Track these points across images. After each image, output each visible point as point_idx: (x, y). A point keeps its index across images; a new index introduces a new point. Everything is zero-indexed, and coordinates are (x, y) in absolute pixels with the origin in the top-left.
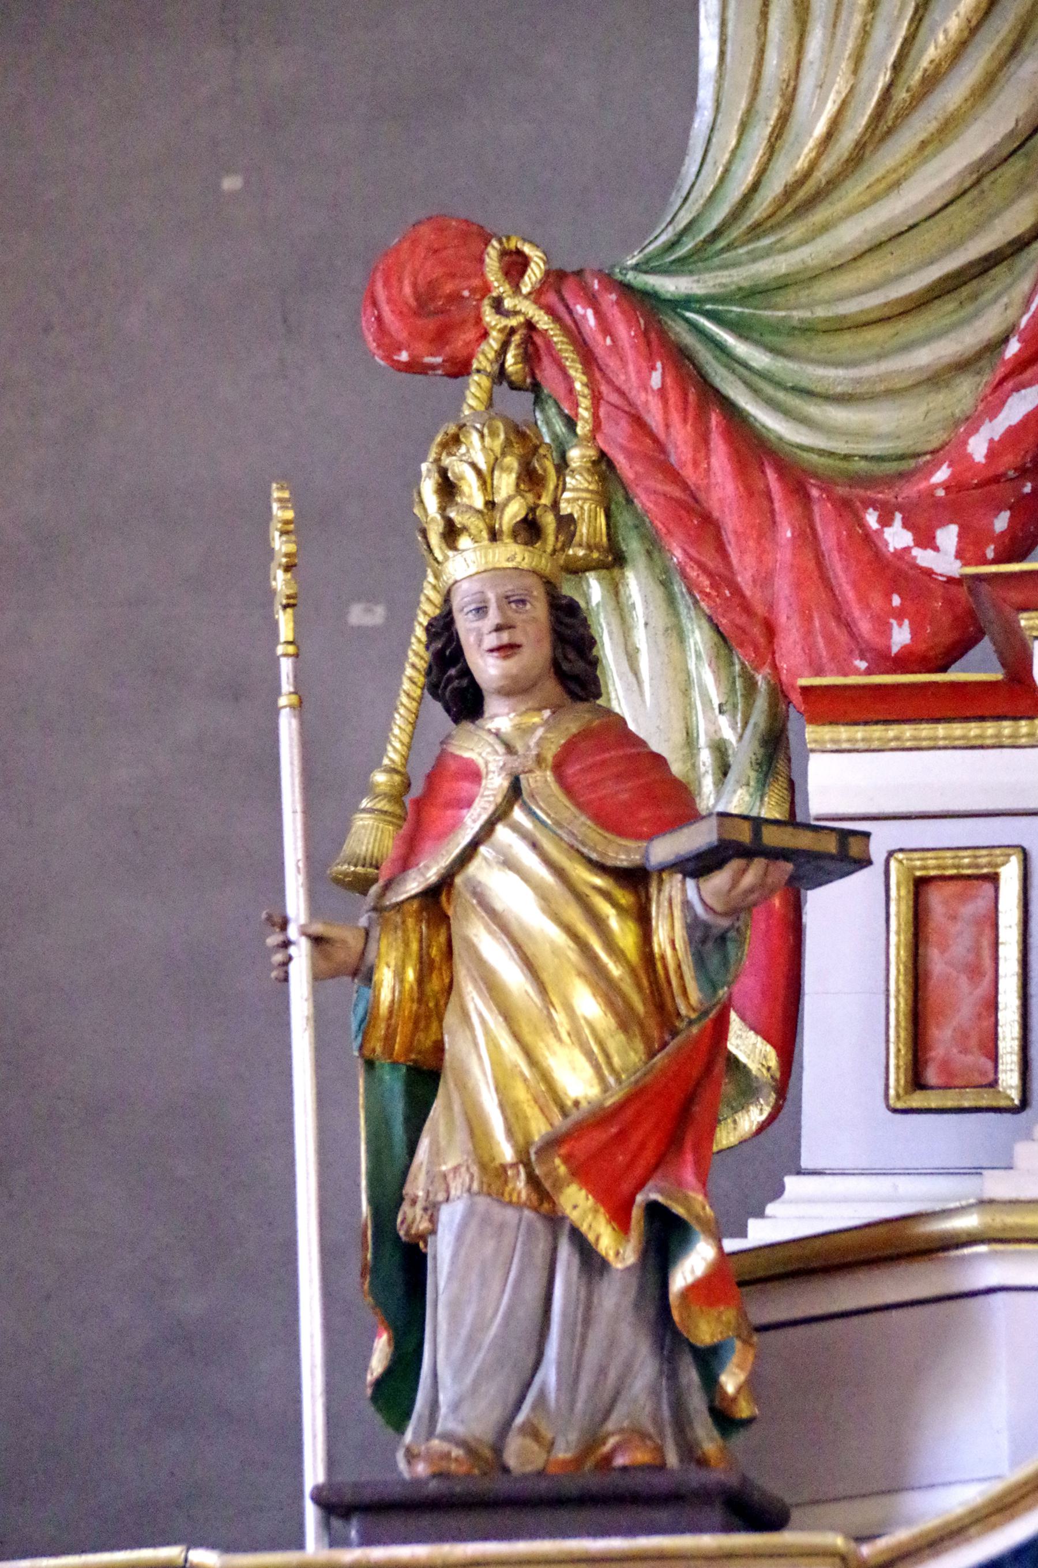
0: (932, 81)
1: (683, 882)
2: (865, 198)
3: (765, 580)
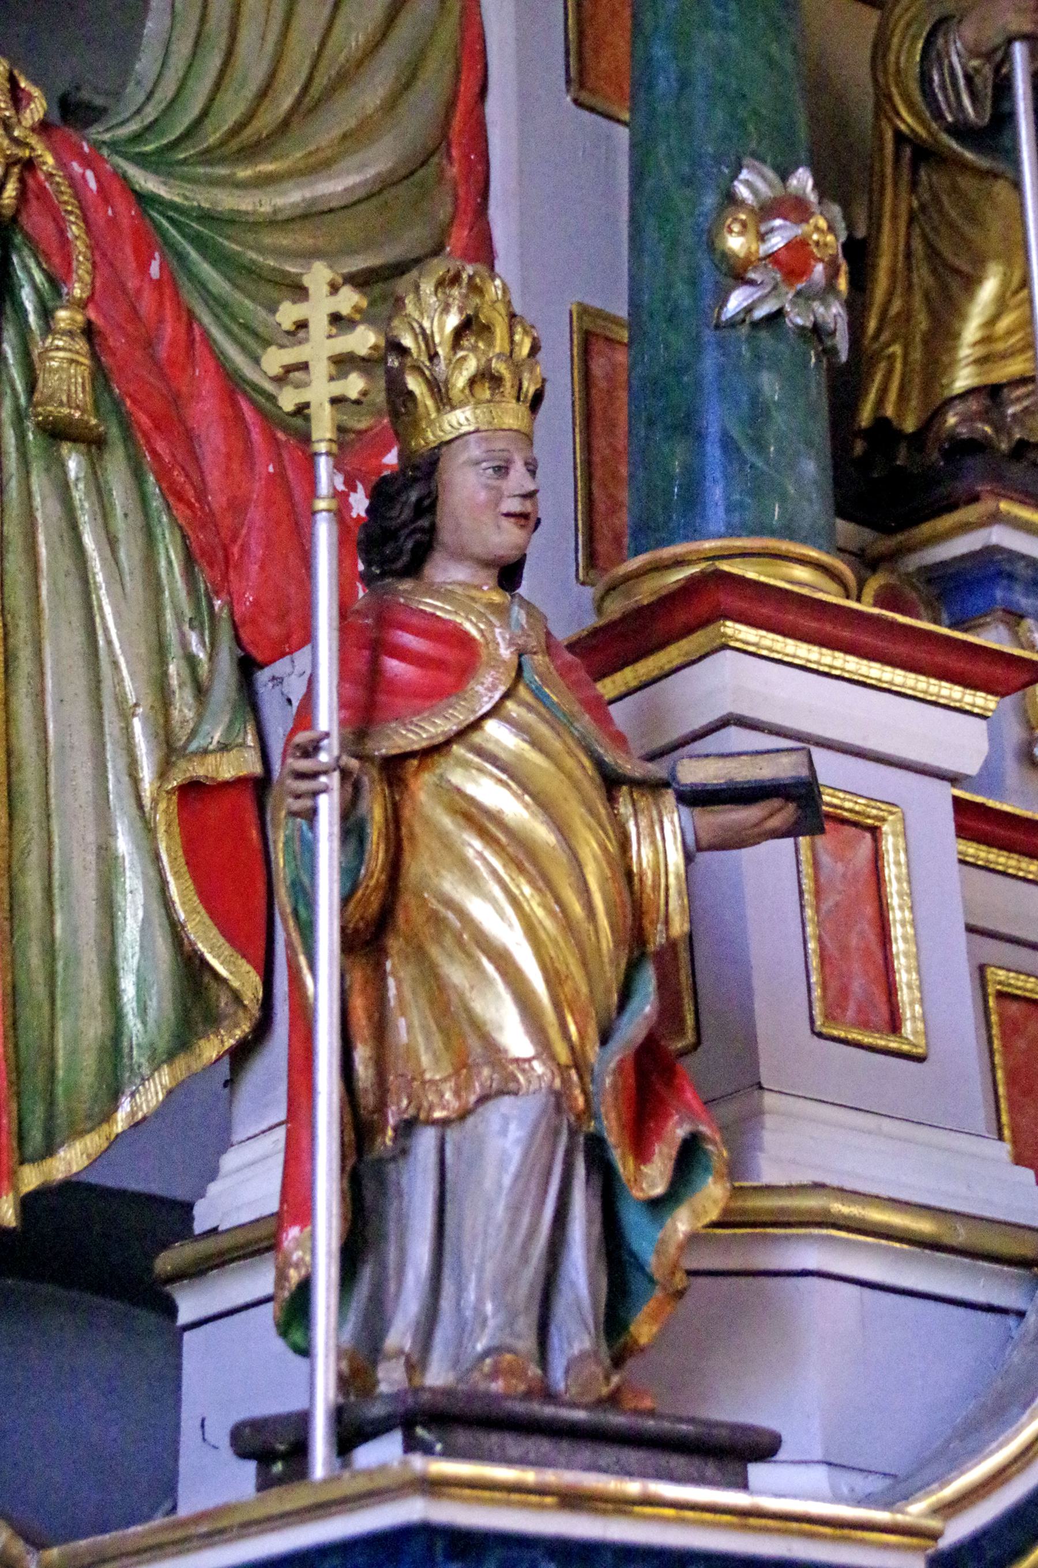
0: (344, 79)
1: (631, 794)
2: (301, 165)
3: (237, 506)
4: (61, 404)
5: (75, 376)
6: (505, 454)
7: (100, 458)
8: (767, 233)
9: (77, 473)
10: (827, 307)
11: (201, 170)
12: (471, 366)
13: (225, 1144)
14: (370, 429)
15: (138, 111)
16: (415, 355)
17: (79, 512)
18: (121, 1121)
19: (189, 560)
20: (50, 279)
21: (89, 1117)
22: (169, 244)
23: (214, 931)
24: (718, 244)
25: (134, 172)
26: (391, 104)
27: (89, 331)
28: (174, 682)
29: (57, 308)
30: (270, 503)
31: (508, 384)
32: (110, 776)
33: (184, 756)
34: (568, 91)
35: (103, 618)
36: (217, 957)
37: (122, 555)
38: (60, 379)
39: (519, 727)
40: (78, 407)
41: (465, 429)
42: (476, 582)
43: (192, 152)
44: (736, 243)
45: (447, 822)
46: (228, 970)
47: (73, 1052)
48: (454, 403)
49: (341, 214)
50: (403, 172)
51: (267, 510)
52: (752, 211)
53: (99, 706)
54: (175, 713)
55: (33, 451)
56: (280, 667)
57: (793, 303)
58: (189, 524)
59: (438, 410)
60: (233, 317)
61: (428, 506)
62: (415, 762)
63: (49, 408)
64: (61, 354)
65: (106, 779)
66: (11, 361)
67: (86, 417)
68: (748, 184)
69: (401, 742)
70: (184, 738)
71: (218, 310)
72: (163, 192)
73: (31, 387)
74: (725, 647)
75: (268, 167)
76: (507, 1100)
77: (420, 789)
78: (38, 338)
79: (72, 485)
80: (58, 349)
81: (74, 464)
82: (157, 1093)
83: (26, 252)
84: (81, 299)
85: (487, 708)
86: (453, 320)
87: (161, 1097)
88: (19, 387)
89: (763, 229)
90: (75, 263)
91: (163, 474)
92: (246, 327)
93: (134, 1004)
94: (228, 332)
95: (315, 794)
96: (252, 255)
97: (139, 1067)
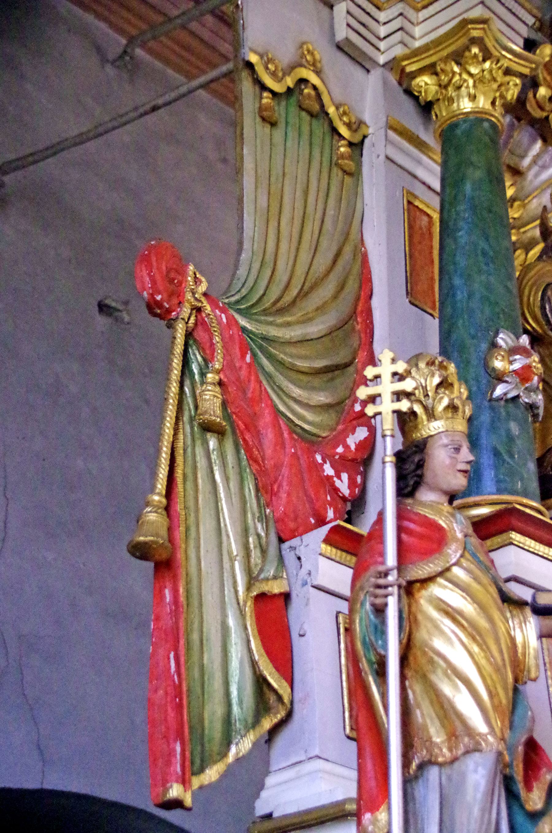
2: (301, 319)
3: (278, 467)
4: (211, 415)
5: (216, 403)
6: (459, 442)
7: (223, 440)
8: (512, 361)
9: (214, 446)
10: (537, 395)
11: (263, 318)
12: (445, 402)
13: (267, 773)
14: (328, 436)
15: (239, 291)
16: (417, 395)
17: (214, 465)
18: (231, 757)
19: (257, 490)
20: (205, 360)
21: (218, 754)
22: (251, 350)
23: (271, 665)
24: (491, 365)
25: (237, 316)
26: (335, 297)
27: (220, 383)
28: (252, 546)
29: (208, 373)
30: (291, 466)
31: (460, 410)
32: (226, 588)
33: (258, 581)
34: (407, 297)
35: (223, 514)
36: (272, 678)
37: (231, 485)
38: (210, 403)
39: (467, 570)
40: (218, 417)
41: (440, 430)
42: (442, 501)
43: (259, 310)
44: (499, 364)
45: (435, 614)
46: (277, 684)
47: (211, 722)
48: (436, 417)
49: (315, 341)
50: (338, 326)
51: (291, 469)
52: (505, 350)
53: (222, 555)
54: (252, 560)
55: (197, 436)
56: (295, 542)
57: (524, 393)
58: (258, 473)
59: (428, 420)
60: (275, 383)
61: (420, 465)
62: (418, 585)
63: (206, 416)
64: (210, 393)
65: (224, 590)
66: (188, 395)
67: (221, 422)
68: (502, 338)
69: (415, 574)
70: (256, 573)
71: (269, 379)
72: (248, 326)
73: (196, 407)
74: (512, 544)
75: (289, 319)
76: (477, 754)
77: (421, 597)
78: (199, 386)
79: (211, 452)
80: (209, 390)
81: (212, 443)
82: (248, 744)
83: (194, 348)
84: (218, 369)
85: (454, 561)
86: (437, 380)
87: (250, 745)
88: (192, 407)
89: (511, 359)
90: (216, 354)
91: (248, 451)
92: (279, 387)
93: (237, 700)
94: (273, 389)
95: (386, 596)
96: (282, 356)
97: (240, 730)
